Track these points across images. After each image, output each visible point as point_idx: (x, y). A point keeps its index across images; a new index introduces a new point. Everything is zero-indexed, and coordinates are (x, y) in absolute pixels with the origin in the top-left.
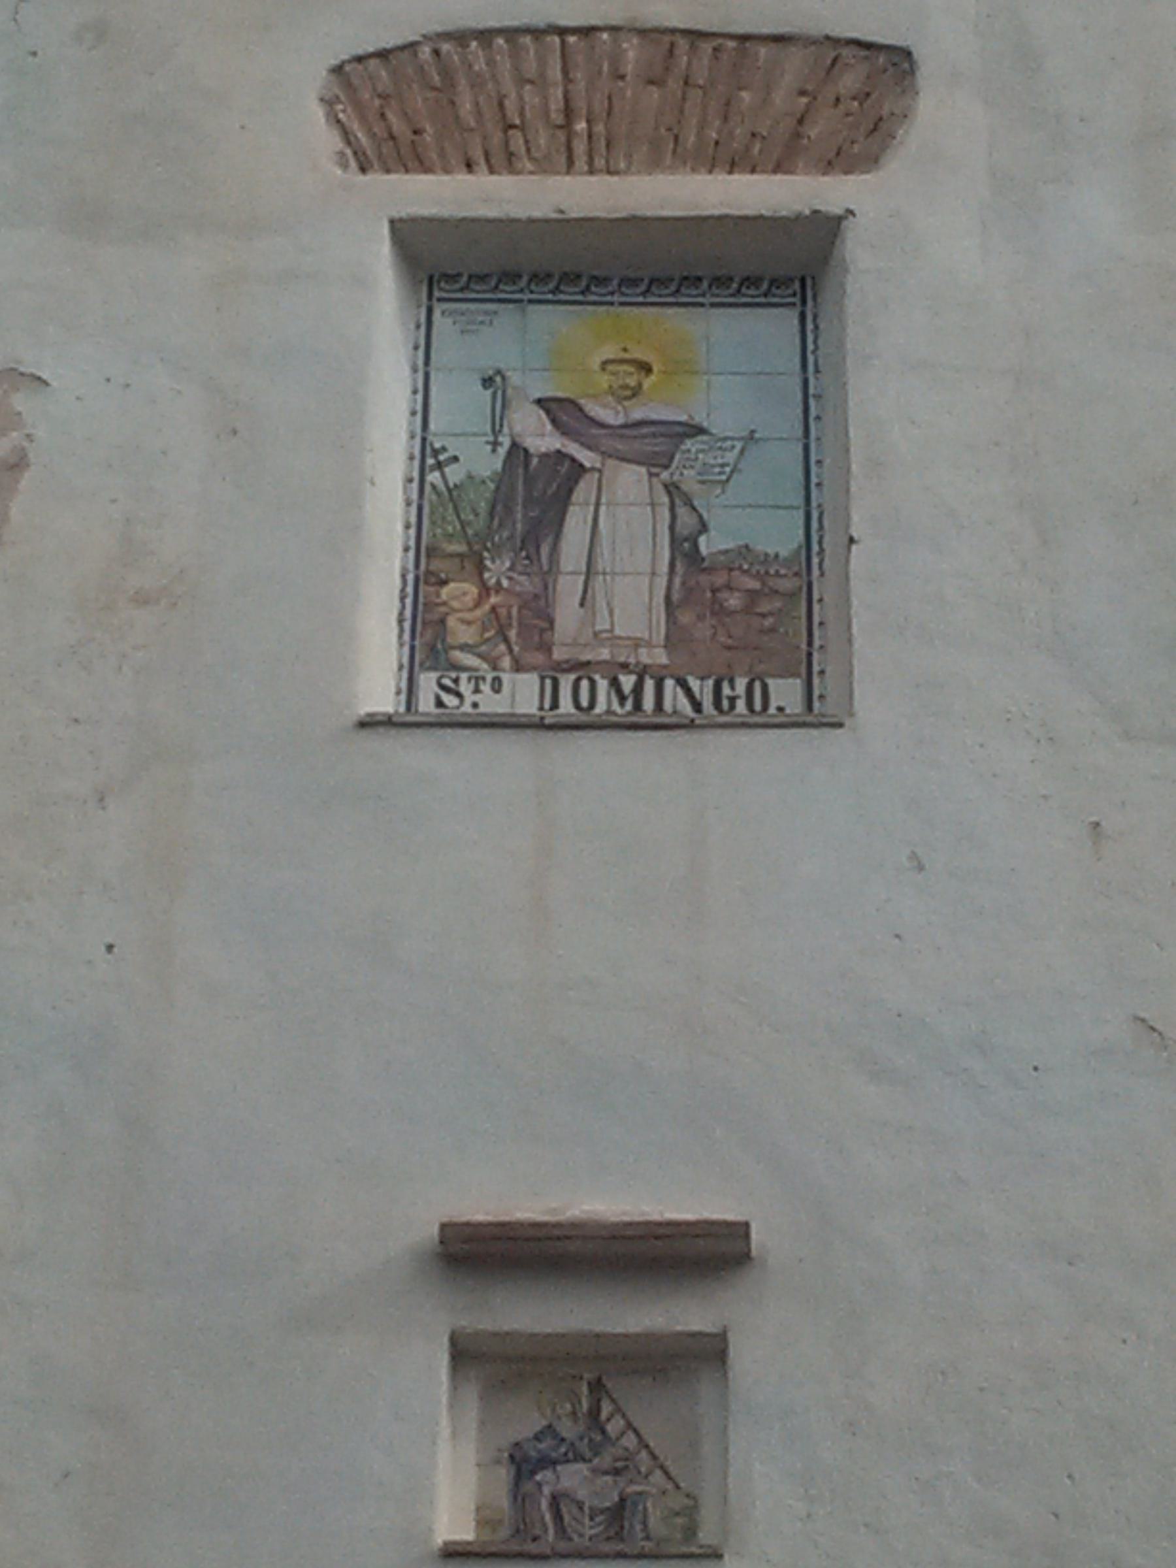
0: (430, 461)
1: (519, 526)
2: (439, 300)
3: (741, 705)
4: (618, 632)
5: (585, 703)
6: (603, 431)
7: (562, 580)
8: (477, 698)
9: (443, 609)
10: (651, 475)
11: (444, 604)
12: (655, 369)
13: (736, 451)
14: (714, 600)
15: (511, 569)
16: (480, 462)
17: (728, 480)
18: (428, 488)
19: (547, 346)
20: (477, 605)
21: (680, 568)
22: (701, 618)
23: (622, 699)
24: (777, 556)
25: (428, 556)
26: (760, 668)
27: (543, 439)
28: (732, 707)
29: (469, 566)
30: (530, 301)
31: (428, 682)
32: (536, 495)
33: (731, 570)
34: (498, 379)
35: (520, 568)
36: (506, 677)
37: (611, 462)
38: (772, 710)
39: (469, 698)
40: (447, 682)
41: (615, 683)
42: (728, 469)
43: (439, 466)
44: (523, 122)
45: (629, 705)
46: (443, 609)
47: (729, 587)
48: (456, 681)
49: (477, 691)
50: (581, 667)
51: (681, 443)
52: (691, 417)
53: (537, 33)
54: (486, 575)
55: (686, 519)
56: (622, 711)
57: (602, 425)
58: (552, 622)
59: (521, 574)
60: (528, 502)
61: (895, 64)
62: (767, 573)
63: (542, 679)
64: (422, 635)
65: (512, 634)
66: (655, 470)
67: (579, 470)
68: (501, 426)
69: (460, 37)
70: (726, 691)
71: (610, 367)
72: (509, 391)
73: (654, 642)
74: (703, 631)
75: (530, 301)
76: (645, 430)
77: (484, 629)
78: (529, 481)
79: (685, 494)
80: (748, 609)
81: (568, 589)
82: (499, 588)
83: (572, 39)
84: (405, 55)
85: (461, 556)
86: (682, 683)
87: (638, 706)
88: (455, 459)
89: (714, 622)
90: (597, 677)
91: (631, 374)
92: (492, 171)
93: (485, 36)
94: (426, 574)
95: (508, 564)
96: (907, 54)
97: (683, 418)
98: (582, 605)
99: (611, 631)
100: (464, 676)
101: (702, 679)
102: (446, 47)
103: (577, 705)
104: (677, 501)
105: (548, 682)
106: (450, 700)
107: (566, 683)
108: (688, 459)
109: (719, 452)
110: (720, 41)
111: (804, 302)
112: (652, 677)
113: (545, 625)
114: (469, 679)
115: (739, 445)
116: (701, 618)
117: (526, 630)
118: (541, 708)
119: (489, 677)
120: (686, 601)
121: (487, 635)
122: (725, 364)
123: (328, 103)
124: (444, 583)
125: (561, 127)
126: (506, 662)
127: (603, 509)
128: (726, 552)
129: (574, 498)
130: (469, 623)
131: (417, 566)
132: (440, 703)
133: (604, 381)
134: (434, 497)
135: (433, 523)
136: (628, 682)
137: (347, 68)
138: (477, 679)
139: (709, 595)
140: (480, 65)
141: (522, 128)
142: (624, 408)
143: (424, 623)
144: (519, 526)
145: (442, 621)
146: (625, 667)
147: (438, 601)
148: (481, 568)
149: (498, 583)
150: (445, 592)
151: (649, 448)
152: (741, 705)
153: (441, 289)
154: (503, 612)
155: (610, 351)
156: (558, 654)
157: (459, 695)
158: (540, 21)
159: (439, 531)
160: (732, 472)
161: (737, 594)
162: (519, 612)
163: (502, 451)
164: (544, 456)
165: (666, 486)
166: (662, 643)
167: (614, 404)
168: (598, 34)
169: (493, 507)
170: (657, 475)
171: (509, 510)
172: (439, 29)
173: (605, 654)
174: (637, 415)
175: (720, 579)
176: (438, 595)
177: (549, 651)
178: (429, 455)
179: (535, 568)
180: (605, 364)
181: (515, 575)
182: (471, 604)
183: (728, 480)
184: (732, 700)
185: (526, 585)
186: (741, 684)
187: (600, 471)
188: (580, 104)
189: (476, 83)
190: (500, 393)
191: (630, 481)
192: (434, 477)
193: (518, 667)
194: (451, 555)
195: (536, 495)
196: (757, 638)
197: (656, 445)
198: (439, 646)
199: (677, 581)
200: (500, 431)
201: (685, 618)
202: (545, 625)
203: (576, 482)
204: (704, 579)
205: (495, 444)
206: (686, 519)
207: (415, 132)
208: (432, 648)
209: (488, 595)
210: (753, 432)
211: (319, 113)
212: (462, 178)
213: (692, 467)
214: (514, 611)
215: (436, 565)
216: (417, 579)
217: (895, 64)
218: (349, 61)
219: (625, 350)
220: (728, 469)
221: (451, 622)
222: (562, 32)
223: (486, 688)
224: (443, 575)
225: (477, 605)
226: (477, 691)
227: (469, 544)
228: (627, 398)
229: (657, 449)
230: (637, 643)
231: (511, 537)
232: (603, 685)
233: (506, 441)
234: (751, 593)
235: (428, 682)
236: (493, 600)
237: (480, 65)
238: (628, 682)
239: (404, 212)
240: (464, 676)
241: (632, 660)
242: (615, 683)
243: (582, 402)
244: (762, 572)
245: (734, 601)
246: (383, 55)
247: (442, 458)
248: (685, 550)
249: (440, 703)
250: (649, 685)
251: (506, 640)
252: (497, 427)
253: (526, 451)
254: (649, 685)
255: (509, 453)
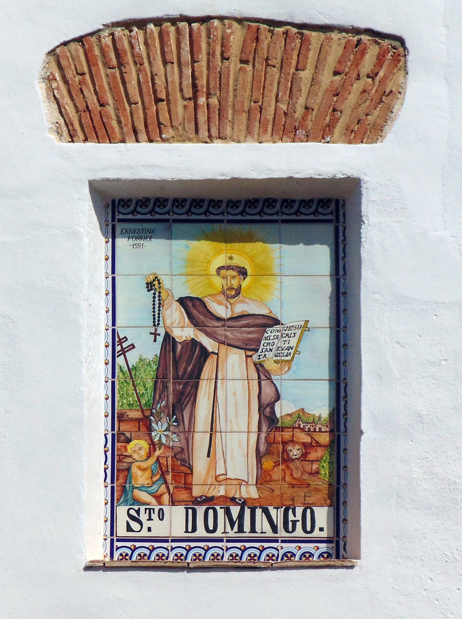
0: (118, 348)
1: (171, 397)
2: (120, 221)
3: (299, 525)
4: (230, 475)
5: (211, 528)
6: (219, 324)
7: (197, 436)
8: (150, 524)
9: (129, 460)
10: (247, 356)
11: (130, 456)
12: (249, 273)
13: (297, 336)
14: (284, 451)
15: (167, 429)
16: (146, 350)
17: (293, 358)
18: (117, 370)
19: (181, 261)
20: (149, 456)
21: (264, 428)
22: (277, 464)
23: (232, 524)
24: (320, 418)
25: (119, 421)
26: (309, 500)
27: (184, 332)
28: (294, 529)
29: (143, 428)
30: (175, 221)
31: (122, 512)
32: (181, 370)
33: (294, 428)
34: (156, 283)
35: (172, 429)
36: (166, 509)
37: (224, 348)
38: (317, 529)
39: (146, 524)
40: (133, 513)
41: (228, 513)
42: (292, 351)
43: (123, 352)
44: (168, 94)
45: (236, 528)
46: (129, 460)
47: (292, 441)
48: (138, 512)
49: (150, 519)
50: (208, 501)
51: (265, 331)
52: (271, 312)
53: (174, 21)
54: (153, 434)
55: (268, 391)
56: (232, 534)
57: (219, 319)
58: (191, 468)
59: (174, 433)
60: (176, 377)
61: (393, 48)
62: (315, 431)
63: (187, 509)
64: (117, 480)
65: (169, 477)
66: (250, 353)
67: (203, 350)
68: (159, 321)
69: (128, 25)
70: (291, 517)
71: (223, 272)
72: (163, 295)
73: (250, 483)
74: (277, 474)
75: (175, 221)
76: (244, 322)
77: (153, 475)
78: (176, 363)
79: (267, 371)
80: (304, 456)
81: (200, 441)
82: (160, 443)
83: (195, 25)
84: (93, 39)
85: (139, 420)
86: (266, 512)
87: (241, 530)
88: (133, 346)
89: (284, 467)
90: (218, 508)
91: (233, 277)
92: (151, 141)
93: (141, 23)
94: (118, 440)
95: (165, 426)
96: (401, 41)
97: (265, 312)
98: (208, 456)
99: (226, 474)
100: (142, 508)
101: (277, 508)
102: (118, 31)
103: (207, 530)
104: (263, 377)
105: (190, 511)
106: (135, 525)
107: (201, 510)
108: (268, 344)
109: (287, 338)
110: (288, 27)
111: (338, 220)
112: (248, 508)
113: (189, 471)
114: (146, 509)
115: (298, 332)
116: (277, 464)
117: (176, 471)
118: (187, 531)
119: (157, 508)
120: (268, 452)
121: (154, 479)
122: (292, 277)
123: (50, 79)
124: (128, 441)
125: (190, 99)
126: (166, 498)
127: (219, 382)
128: (290, 415)
129: (202, 377)
130: (144, 470)
131: (113, 429)
132: (129, 529)
133: (218, 282)
134: (121, 375)
135: (122, 396)
136: (235, 511)
137: (58, 51)
138: (150, 509)
139: (281, 446)
140: (141, 49)
141: (168, 101)
142: (231, 304)
143: (118, 470)
144: (171, 397)
145: (128, 470)
146: (233, 500)
147: (125, 454)
148: (150, 429)
149: (160, 440)
150: (130, 446)
151: (246, 336)
152: (299, 525)
153: (120, 212)
154: (163, 461)
155: (221, 260)
156: (197, 491)
157: (141, 523)
158: (174, 12)
159: (125, 401)
160: (294, 354)
161: (297, 447)
162: (173, 461)
163: (160, 339)
164: (185, 343)
165: (255, 365)
166: (255, 484)
167: (225, 302)
168: (212, 21)
169: (156, 383)
170: (251, 356)
171: (165, 387)
172: (114, 20)
173: (221, 491)
174: (239, 309)
175: (287, 435)
176: (126, 448)
177: (190, 489)
178: (118, 345)
179: (181, 429)
180: (220, 269)
181: (170, 434)
182: (145, 457)
183: (293, 358)
184: (294, 523)
185: (176, 440)
186: (299, 511)
187: (217, 354)
188: (202, 82)
189: (138, 63)
190: (157, 294)
191: (234, 362)
192: (120, 361)
193: (173, 503)
194: (132, 420)
195: (181, 370)
196: (315, 481)
197: (249, 333)
198: (127, 486)
199: (263, 436)
200: (158, 324)
201: (268, 464)
202: (189, 471)
203: (205, 361)
204: (278, 436)
205: (156, 334)
206: (268, 391)
207: (102, 105)
208: (123, 489)
209: (155, 451)
210: (307, 322)
211: (40, 89)
212: (131, 146)
213: (271, 350)
214: (170, 462)
215: (124, 427)
216: (113, 435)
217: (393, 48)
218: (58, 46)
219: (231, 258)
220: (292, 351)
221: (134, 469)
222: (190, 20)
223: (155, 516)
224: (128, 435)
225: (149, 456)
226: (150, 519)
227: (142, 411)
228: (233, 297)
229: (250, 336)
230: (240, 482)
231: (167, 405)
232: (221, 513)
233: (161, 331)
234: (305, 445)
235: (122, 512)
236: (157, 453)
237: (141, 49)
238: (235, 511)
239: (99, 175)
240: (142, 508)
241: (237, 496)
242: (228, 513)
243: (206, 300)
244: (312, 430)
245: (295, 452)
246: (80, 40)
247: (125, 345)
248: (267, 415)
249: (129, 529)
250: (247, 512)
251: (166, 482)
252: (157, 323)
253: (173, 338)
254: (247, 512)
255: (165, 340)
